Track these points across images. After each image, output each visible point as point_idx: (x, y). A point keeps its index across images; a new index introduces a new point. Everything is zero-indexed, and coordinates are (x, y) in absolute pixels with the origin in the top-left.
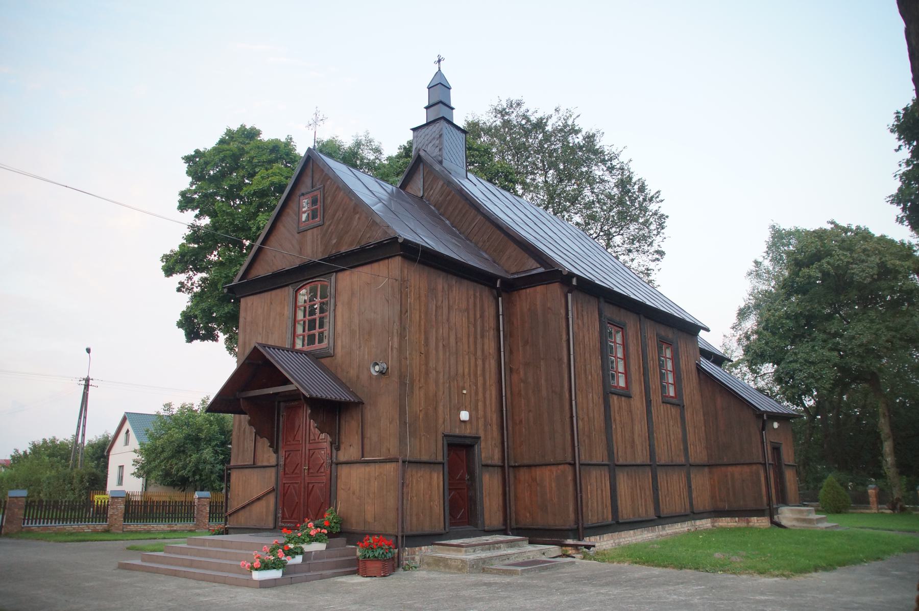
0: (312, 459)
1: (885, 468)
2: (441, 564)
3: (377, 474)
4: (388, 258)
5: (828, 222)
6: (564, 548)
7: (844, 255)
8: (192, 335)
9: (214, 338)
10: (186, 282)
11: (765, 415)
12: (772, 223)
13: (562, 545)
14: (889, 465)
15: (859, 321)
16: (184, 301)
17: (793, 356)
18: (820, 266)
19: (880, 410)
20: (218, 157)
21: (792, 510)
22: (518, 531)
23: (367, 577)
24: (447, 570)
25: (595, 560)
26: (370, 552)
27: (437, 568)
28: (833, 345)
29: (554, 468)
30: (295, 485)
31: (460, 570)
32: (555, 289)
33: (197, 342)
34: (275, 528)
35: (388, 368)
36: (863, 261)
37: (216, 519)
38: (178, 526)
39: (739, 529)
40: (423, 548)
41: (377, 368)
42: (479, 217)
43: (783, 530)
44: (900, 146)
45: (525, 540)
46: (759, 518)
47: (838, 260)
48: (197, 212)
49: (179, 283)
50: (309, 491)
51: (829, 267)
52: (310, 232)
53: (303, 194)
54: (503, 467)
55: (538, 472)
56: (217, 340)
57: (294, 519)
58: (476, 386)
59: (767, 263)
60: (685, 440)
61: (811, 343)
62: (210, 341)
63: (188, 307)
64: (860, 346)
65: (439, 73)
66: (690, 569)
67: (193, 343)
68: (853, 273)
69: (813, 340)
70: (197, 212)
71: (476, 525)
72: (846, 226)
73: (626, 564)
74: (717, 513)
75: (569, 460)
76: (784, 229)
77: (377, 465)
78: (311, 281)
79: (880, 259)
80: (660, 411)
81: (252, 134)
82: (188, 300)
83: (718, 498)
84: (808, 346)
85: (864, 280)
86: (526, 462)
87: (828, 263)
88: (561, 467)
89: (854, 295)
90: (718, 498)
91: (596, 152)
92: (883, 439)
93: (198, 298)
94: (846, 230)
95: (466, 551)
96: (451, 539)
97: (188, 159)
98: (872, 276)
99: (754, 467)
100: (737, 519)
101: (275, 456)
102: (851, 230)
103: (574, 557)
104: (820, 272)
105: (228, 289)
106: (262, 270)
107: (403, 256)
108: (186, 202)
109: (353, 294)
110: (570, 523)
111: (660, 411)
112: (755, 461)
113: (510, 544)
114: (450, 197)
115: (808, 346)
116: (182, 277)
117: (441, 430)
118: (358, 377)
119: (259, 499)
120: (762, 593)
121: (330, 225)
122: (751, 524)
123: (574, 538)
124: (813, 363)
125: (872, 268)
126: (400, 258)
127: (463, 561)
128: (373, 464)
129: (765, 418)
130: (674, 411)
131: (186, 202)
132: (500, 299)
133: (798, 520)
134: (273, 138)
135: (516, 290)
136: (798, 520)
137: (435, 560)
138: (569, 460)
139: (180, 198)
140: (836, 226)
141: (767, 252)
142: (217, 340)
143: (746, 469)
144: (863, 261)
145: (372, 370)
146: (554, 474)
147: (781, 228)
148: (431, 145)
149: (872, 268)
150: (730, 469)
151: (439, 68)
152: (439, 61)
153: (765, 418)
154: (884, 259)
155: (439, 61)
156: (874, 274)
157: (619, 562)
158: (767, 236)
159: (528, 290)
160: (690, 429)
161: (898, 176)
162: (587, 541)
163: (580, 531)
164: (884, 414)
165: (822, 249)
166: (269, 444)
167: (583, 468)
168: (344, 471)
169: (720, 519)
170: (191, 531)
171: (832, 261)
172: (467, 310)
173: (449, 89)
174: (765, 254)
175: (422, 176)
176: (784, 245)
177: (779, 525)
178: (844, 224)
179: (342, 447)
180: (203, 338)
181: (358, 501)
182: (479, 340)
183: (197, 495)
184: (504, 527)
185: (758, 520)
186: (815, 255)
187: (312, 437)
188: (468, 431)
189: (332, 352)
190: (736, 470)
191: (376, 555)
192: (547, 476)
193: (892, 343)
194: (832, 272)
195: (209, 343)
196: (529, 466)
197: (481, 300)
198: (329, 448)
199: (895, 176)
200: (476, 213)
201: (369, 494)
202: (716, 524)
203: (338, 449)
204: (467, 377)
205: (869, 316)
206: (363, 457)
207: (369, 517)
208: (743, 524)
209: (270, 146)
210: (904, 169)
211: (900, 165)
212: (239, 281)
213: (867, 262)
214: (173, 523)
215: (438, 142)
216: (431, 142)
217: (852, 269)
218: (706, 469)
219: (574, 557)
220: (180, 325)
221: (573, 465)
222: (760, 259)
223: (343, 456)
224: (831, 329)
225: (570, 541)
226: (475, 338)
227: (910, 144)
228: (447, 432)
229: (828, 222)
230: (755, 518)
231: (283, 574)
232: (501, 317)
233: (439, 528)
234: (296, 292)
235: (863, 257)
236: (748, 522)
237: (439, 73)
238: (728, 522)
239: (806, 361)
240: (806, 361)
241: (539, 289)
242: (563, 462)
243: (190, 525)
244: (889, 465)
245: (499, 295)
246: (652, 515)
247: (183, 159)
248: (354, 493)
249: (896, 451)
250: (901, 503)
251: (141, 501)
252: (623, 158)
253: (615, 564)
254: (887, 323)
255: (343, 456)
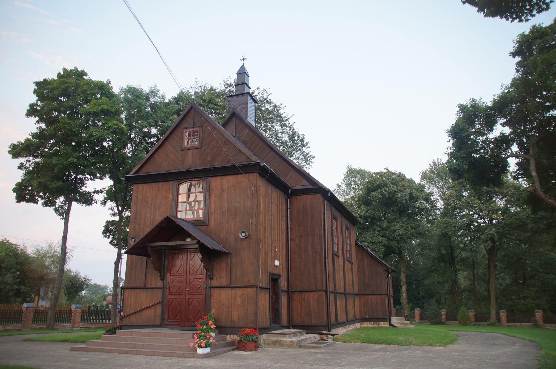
0: (192, 284)
1: (402, 299)
2: (277, 344)
3: (240, 295)
4: (249, 173)
5: (385, 169)
6: (321, 336)
7: (393, 187)
8: (20, 199)
9: (36, 202)
10: (25, 163)
11: (390, 270)
12: (348, 164)
13: (321, 334)
14: (404, 298)
15: (397, 222)
16: (19, 176)
17: (364, 238)
18: (381, 192)
19: (402, 269)
20: (64, 86)
21: (397, 319)
22: (295, 327)
23: (248, 351)
24: (281, 347)
25: (340, 341)
26: (249, 337)
27: (274, 346)
28: (383, 234)
29: (316, 293)
30: (179, 300)
31: (289, 347)
32: (319, 198)
33: (23, 203)
34: (161, 325)
35: (249, 235)
36: (402, 191)
37: (6, 322)
38: (11, 327)
39: (374, 328)
40: (264, 335)
41: (243, 234)
42: (272, 153)
43: (394, 328)
44: (450, 140)
45: (304, 332)
46: (384, 323)
47: (390, 190)
48: (37, 119)
49: (20, 164)
50: (170, 303)
51: (386, 192)
52: (190, 152)
53: (186, 128)
54: (288, 292)
55: (306, 295)
56: (37, 203)
57: (178, 319)
58: (280, 247)
59: (344, 186)
60: (353, 280)
61: (372, 232)
62: (32, 203)
63: (23, 180)
64: (398, 235)
65: (243, 66)
66: (395, 344)
67: (20, 203)
68: (397, 197)
69: (373, 231)
70: (37, 119)
71: (279, 324)
72: (393, 172)
73: (359, 343)
74: (363, 320)
75: (324, 289)
76: (354, 169)
77: (241, 289)
78: (188, 180)
79: (410, 191)
80: (346, 263)
81: (81, 74)
82: (22, 175)
83: (363, 312)
84: (371, 234)
85: (402, 201)
86: (298, 289)
87: (385, 190)
88: (320, 293)
89: (395, 208)
90: (363, 312)
91: (279, 116)
92: (402, 285)
93: (29, 173)
94: (393, 174)
95: (288, 337)
96: (277, 330)
97: (37, 84)
98: (406, 199)
99: (383, 296)
100: (373, 323)
101: (162, 282)
102: (396, 174)
103: (328, 341)
104: (381, 195)
105: (126, 178)
106: (151, 170)
107: (260, 174)
108: (32, 111)
109: (223, 190)
110: (325, 323)
111: (346, 263)
112: (383, 293)
113: (295, 335)
114: (253, 139)
115: (371, 234)
116: (22, 160)
117: (269, 271)
118: (227, 239)
119: (148, 308)
120: (456, 352)
121: (206, 150)
122: (380, 325)
123: (326, 331)
124: (374, 243)
125: (407, 195)
126: (257, 174)
127: (291, 342)
128: (238, 288)
129: (390, 271)
130: (350, 265)
131: (32, 111)
132: (289, 200)
133: (400, 323)
134: (102, 80)
135: (294, 196)
136: (400, 323)
137: (273, 342)
138: (324, 289)
139: (29, 108)
140: (389, 171)
141: (343, 180)
142: (37, 203)
143: (379, 297)
144: (402, 191)
145: (240, 235)
146: (316, 296)
147: (353, 168)
148: (240, 107)
149: (407, 195)
150: (370, 297)
151: (243, 63)
152: (243, 59)
153: (390, 271)
154: (412, 191)
155: (243, 59)
156: (407, 199)
157: (354, 342)
158: (345, 171)
159: (302, 196)
160: (354, 275)
161: (447, 154)
162: (333, 331)
163: (329, 327)
164: (404, 271)
165: (382, 183)
166: (160, 275)
167: (330, 293)
168: (216, 292)
169: (364, 323)
170: (19, 330)
171: (387, 189)
172: (277, 205)
173: (249, 76)
174: (342, 181)
175: (234, 124)
176: (353, 177)
177: (393, 326)
178: (392, 170)
179: (215, 278)
180: (28, 201)
181: (227, 309)
182: (281, 221)
183: (25, 305)
184: (288, 325)
185: (383, 324)
186: (378, 185)
187: (191, 271)
188: (277, 271)
189: (207, 223)
190: (373, 298)
191: (254, 339)
192: (312, 298)
193: (413, 235)
194: (387, 196)
195: (31, 204)
196: (301, 292)
197: (282, 200)
198: (205, 278)
199: (445, 154)
200: (270, 150)
201: (235, 305)
202: (362, 326)
203: (212, 279)
204: (277, 242)
205: (402, 220)
206: (231, 284)
207: (235, 318)
208: (376, 326)
209: (99, 85)
210: (449, 151)
211: (447, 149)
212: (134, 174)
213: (404, 192)
214: (7, 325)
215: (244, 106)
216: (240, 106)
217: (397, 195)
218: (358, 296)
219: (328, 341)
220: (14, 190)
221: (326, 291)
222: (340, 184)
223: (214, 283)
224: (383, 225)
225: (325, 332)
226: (279, 221)
227: (453, 140)
228: (271, 272)
229: (385, 169)
230: (382, 322)
231: (211, 350)
232: (289, 210)
233: (268, 325)
234: (178, 185)
235: (403, 189)
236: (379, 325)
237: (243, 66)
238: (368, 325)
239: (371, 241)
240: (371, 241)
241: (309, 196)
242: (321, 290)
243: (19, 326)
244: (404, 298)
245: (288, 198)
246: (345, 320)
247: (34, 83)
248: (223, 305)
249: (408, 291)
250: (408, 318)
251: (18, 310)
252: (291, 121)
253: (353, 343)
254: (411, 225)
255: (214, 283)
